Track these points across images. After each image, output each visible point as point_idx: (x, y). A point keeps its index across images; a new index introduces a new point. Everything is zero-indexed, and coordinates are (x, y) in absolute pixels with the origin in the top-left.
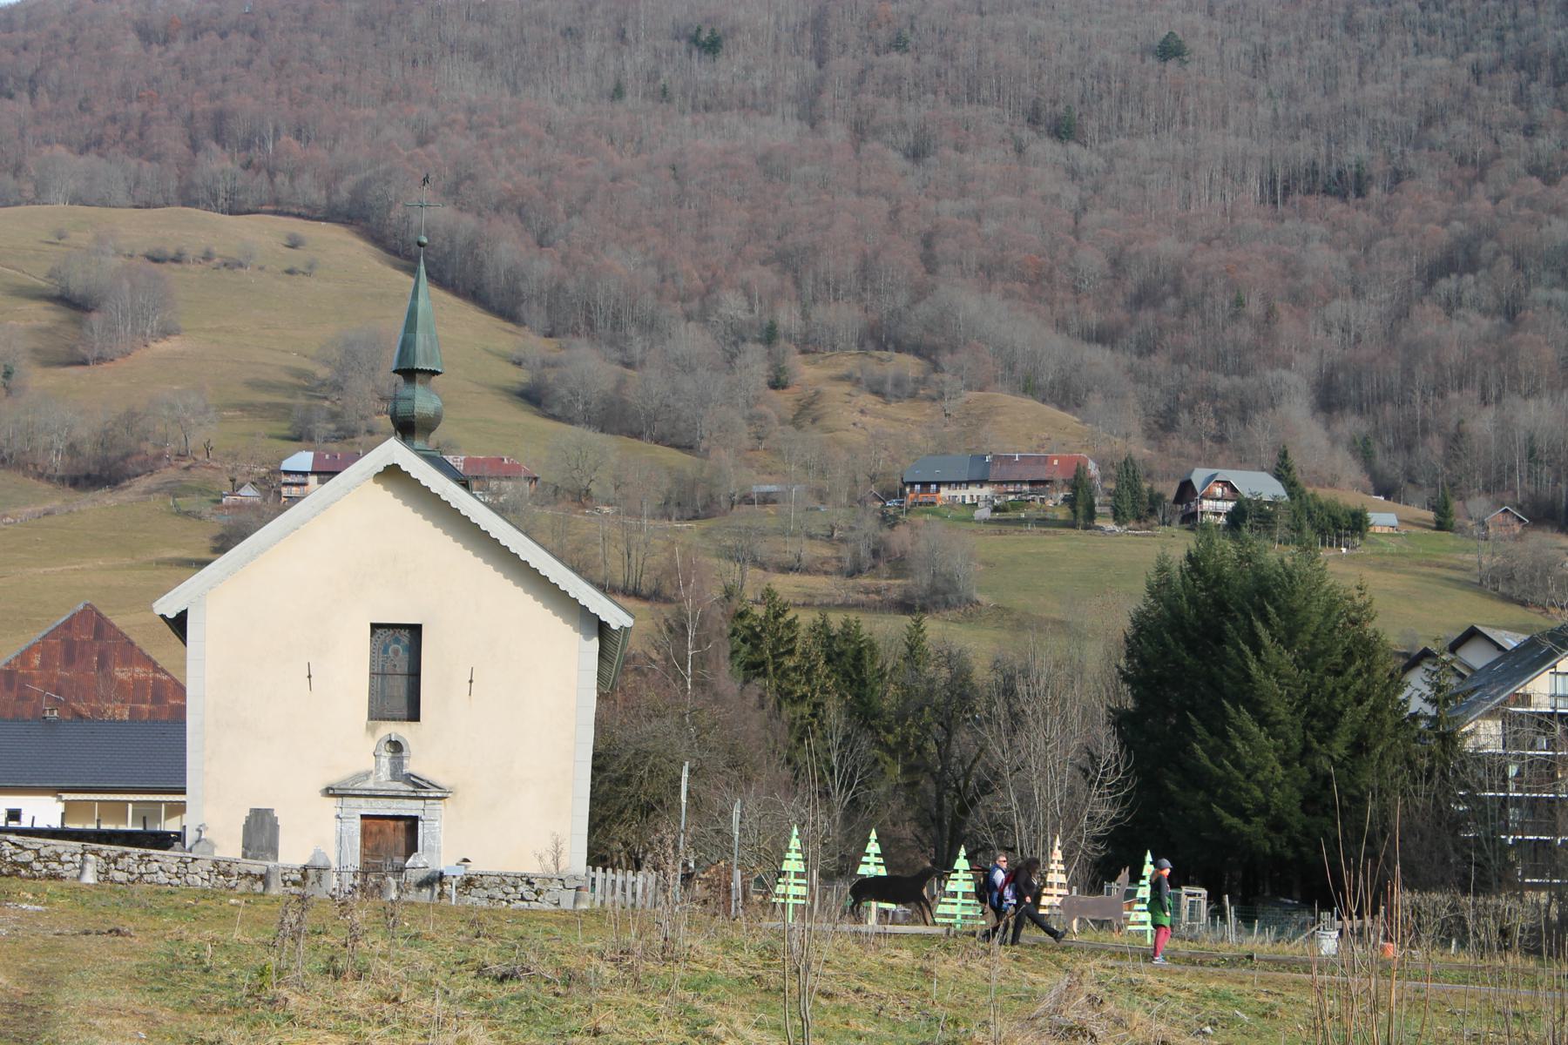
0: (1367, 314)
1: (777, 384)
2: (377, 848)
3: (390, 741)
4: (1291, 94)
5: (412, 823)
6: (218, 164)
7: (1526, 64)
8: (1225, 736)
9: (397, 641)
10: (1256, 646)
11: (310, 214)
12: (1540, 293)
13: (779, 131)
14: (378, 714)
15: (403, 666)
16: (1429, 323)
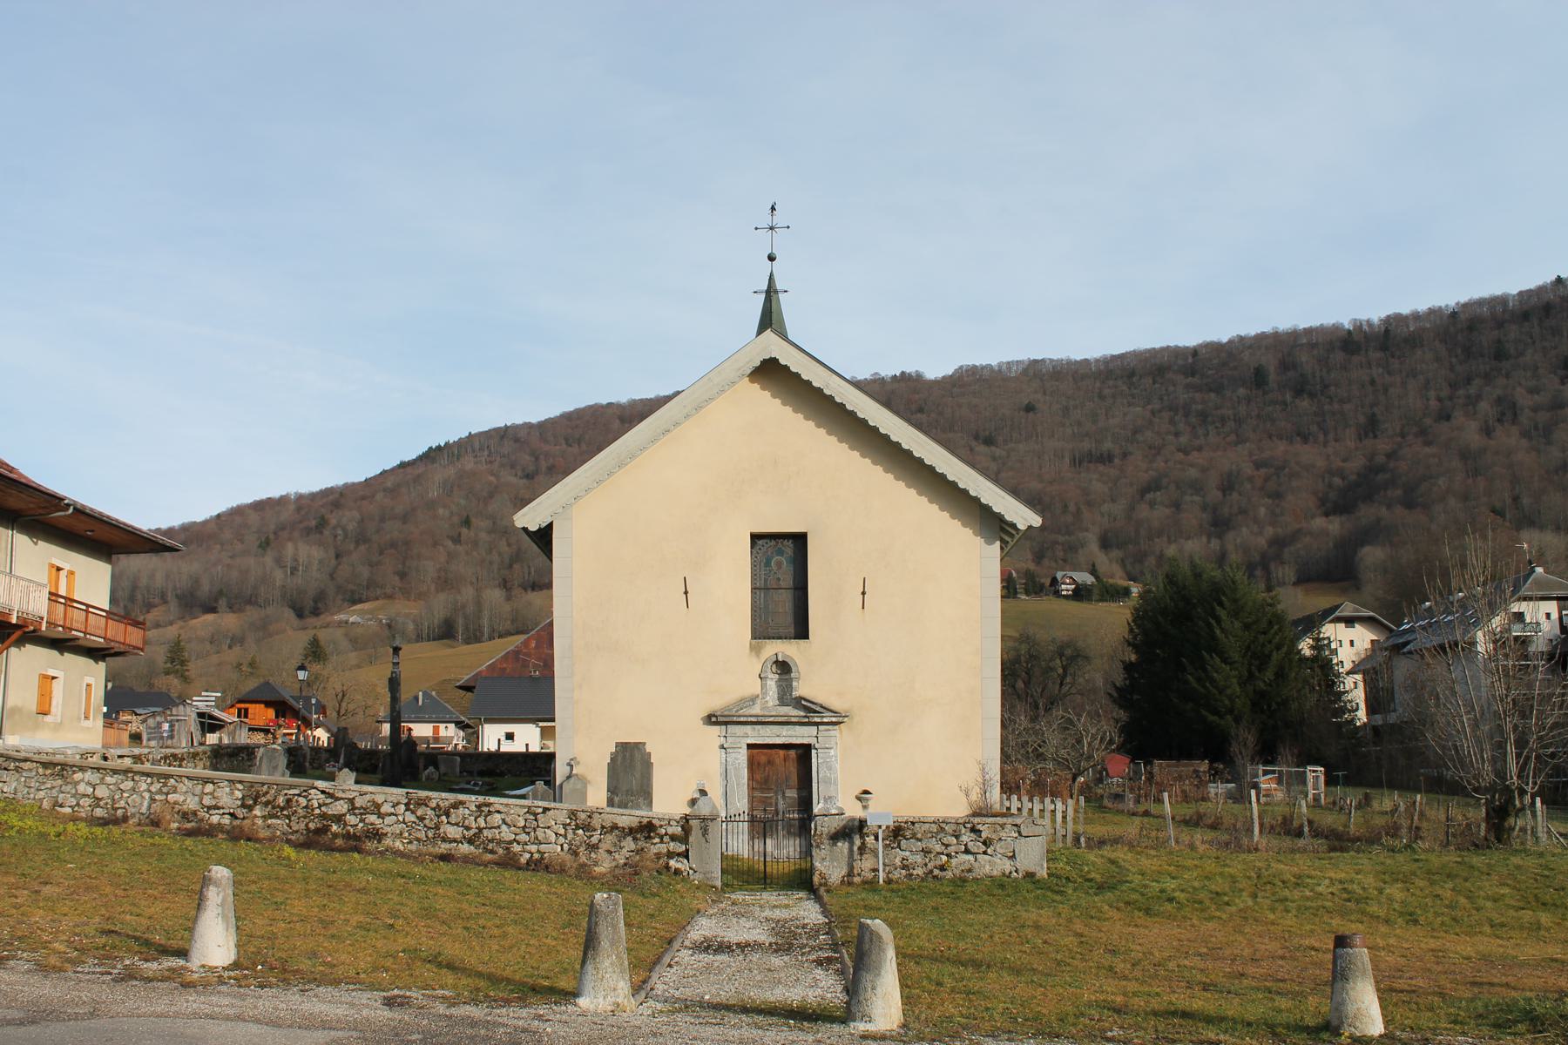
0: (1118, 509)
2: (767, 780)
3: (776, 662)
4: (1079, 424)
5: (804, 752)
7: (1173, 408)
8: (1205, 670)
9: (780, 553)
10: (1218, 621)
12: (1187, 498)
14: (762, 631)
15: (787, 580)
16: (1143, 512)
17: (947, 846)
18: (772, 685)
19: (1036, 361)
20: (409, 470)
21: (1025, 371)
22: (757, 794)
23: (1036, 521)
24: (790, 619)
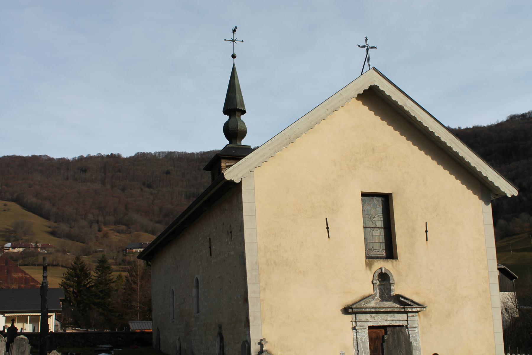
1: (99, 231)
11: (8, 200)
13: (98, 186)
19: (171, 153)
21: (166, 156)
23: (515, 193)
24: (383, 246)
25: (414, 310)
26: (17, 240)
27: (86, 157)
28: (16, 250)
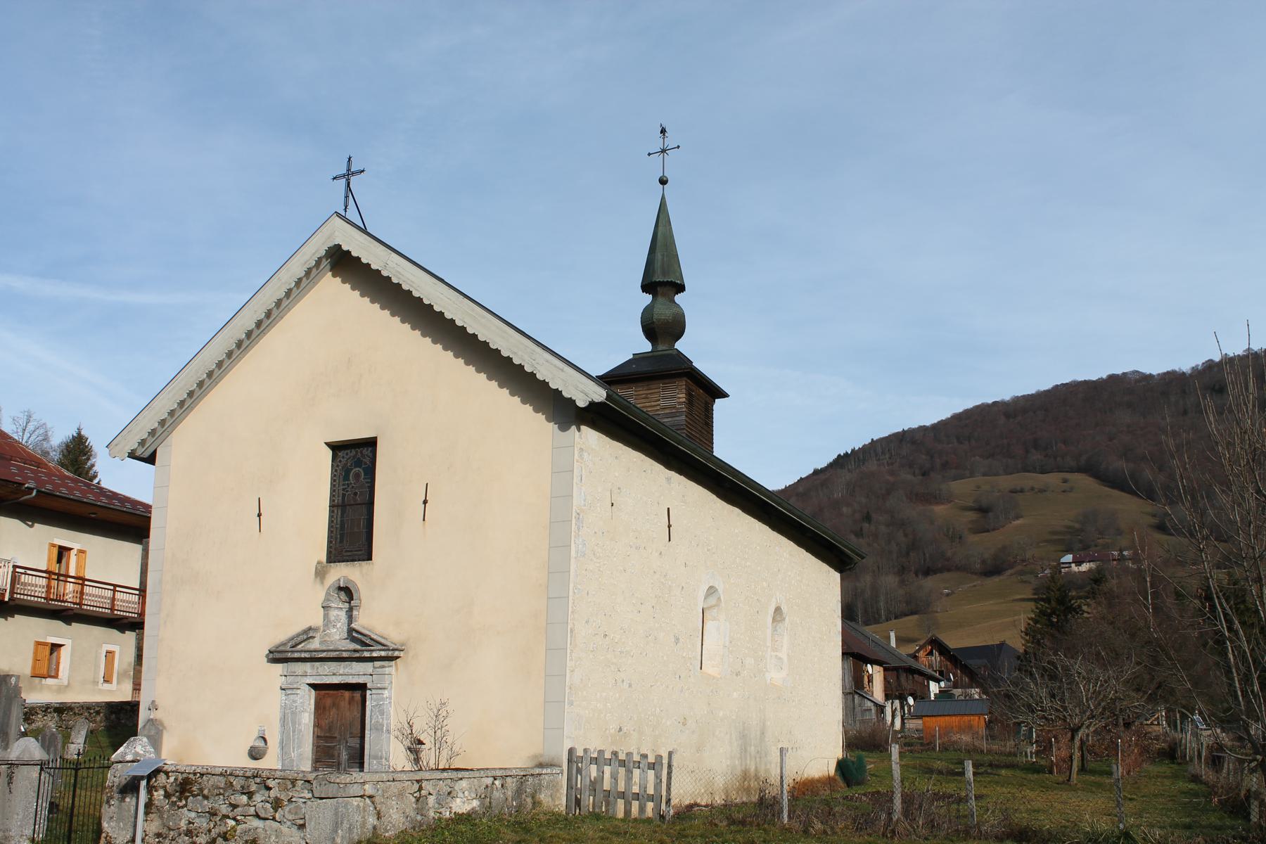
6: (1036, 456)
11: (1071, 471)
17: (234, 806)
18: (339, 615)
20: (822, 477)
22: (322, 743)
25: (375, 654)
26: (1086, 548)
27: (1221, 362)
28: (1085, 567)
